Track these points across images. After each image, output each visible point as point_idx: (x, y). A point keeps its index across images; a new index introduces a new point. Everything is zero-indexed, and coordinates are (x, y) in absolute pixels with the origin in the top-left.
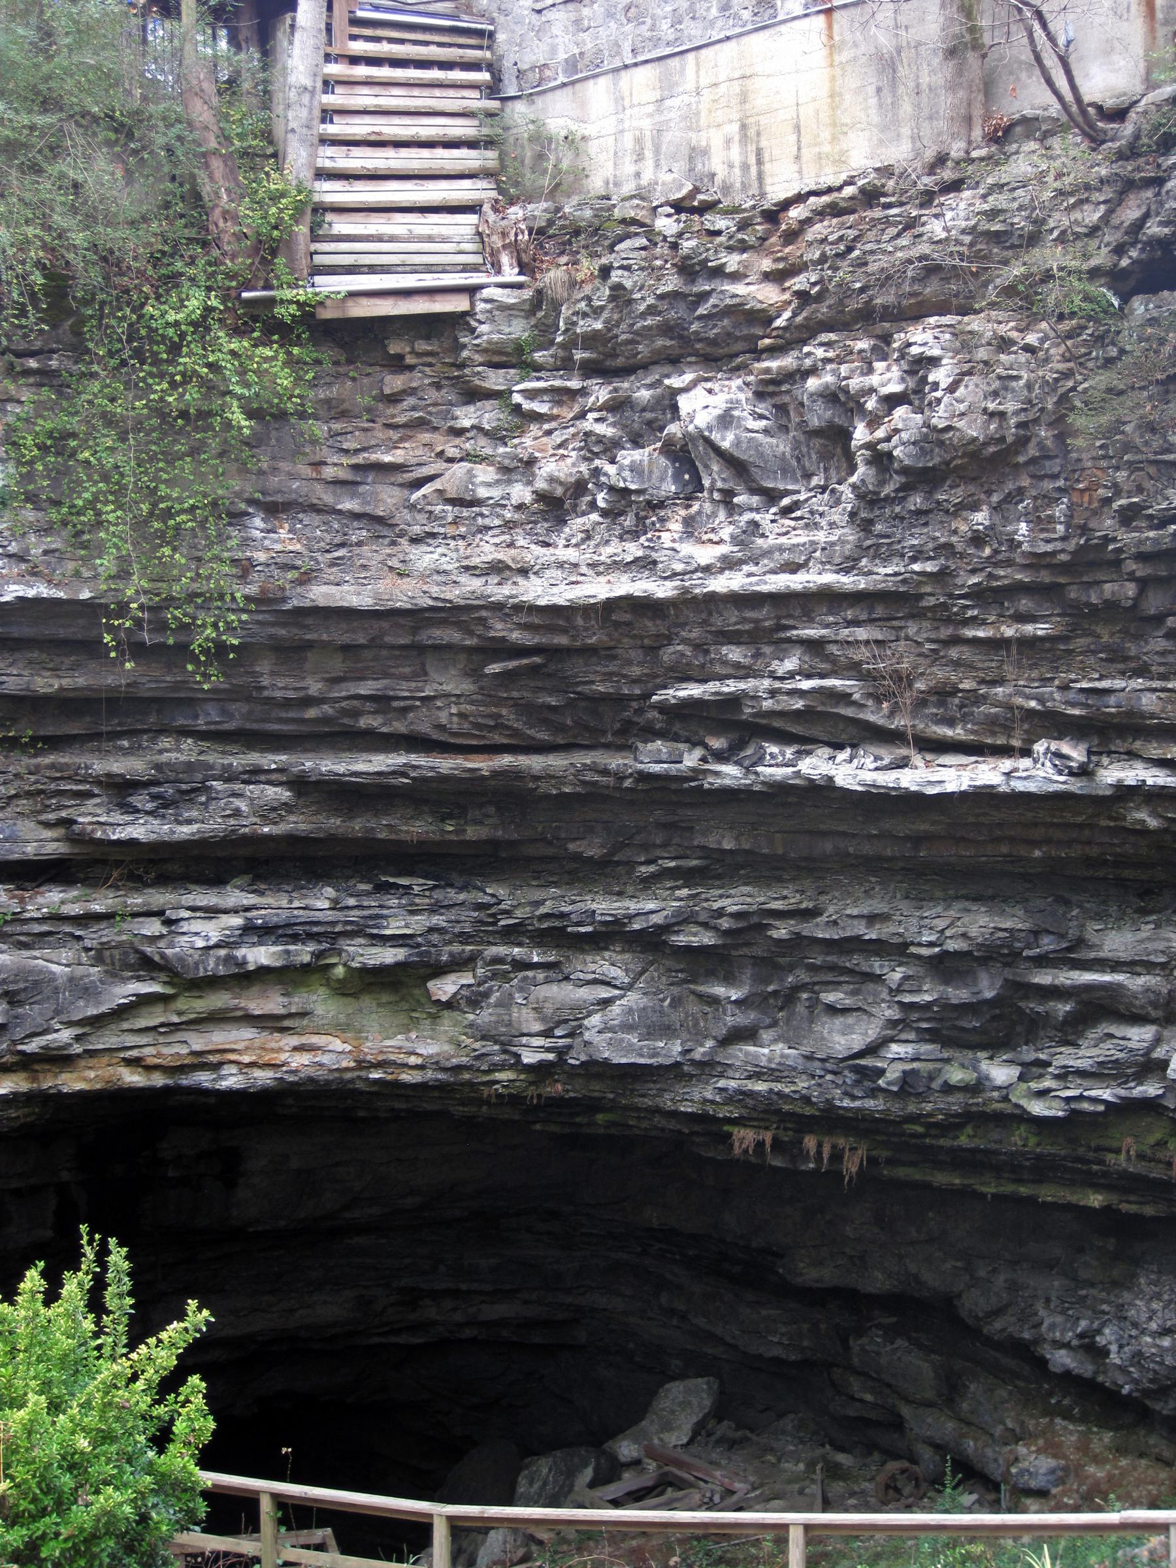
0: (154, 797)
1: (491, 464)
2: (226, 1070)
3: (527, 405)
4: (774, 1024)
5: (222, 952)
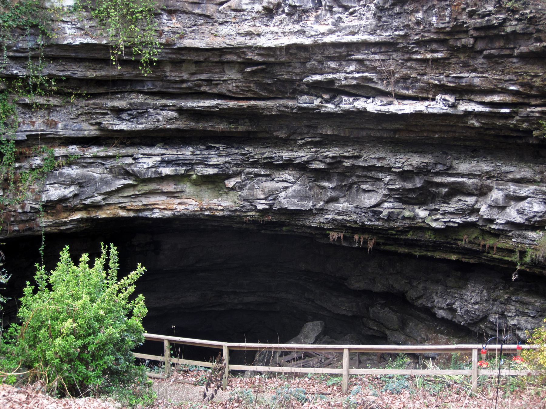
0: (129, 115)
4: (345, 196)
5: (154, 170)
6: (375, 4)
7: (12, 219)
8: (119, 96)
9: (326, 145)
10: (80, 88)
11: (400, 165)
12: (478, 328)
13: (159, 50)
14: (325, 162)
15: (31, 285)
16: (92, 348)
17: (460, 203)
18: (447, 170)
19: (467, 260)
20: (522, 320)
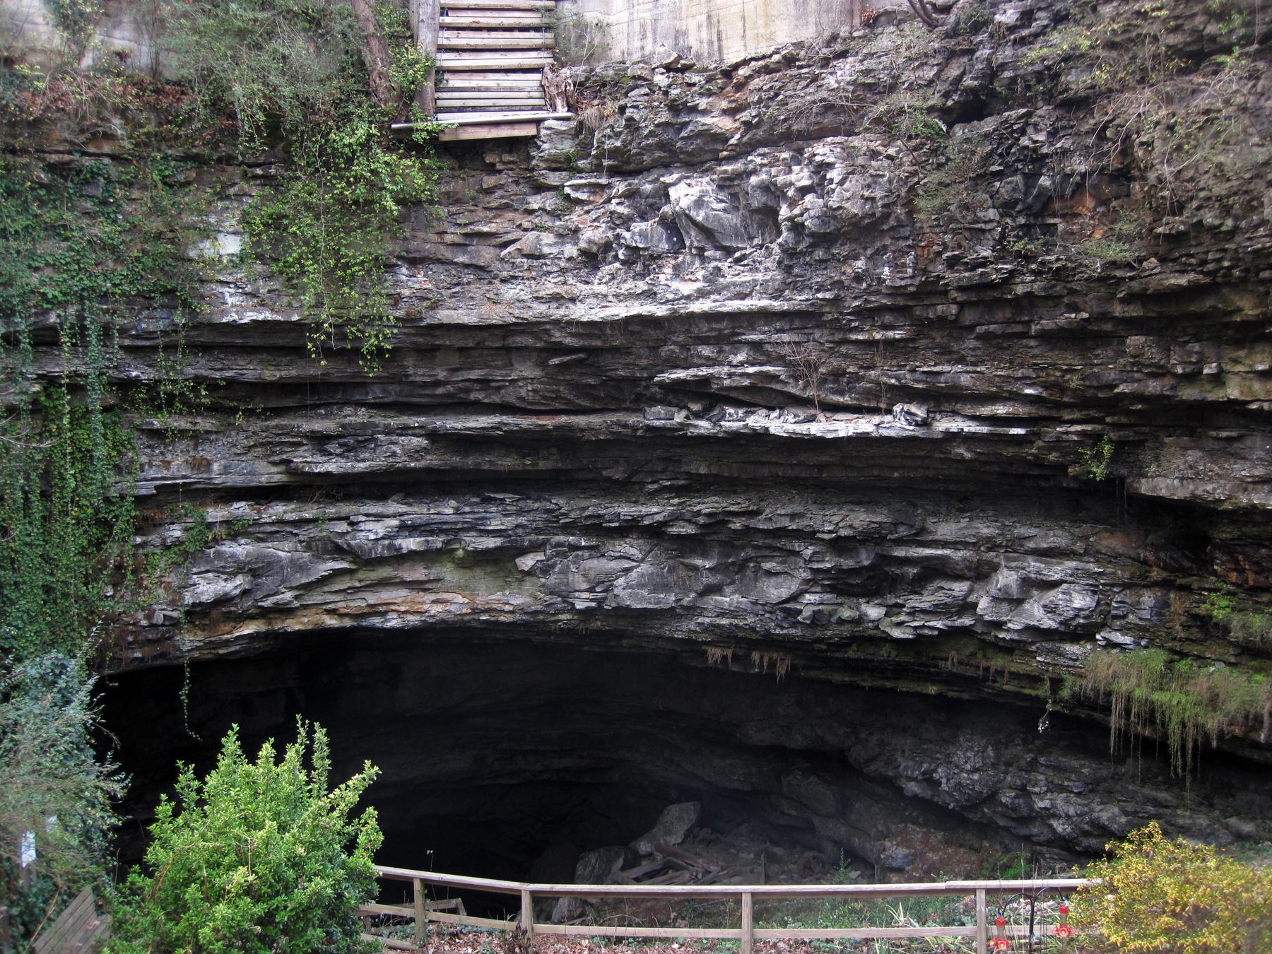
0: (341, 445)
1: (551, 232)
2: (390, 616)
3: (574, 195)
4: (733, 582)
5: (386, 542)
6: (780, 245)
7: (130, 639)
8: (323, 412)
9: (698, 491)
10: (252, 398)
11: (831, 528)
12: (979, 815)
13: (395, 331)
14: (696, 523)
15: (168, 801)
16: (283, 917)
17: (940, 593)
18: (916, 534)
19: (956, 694)
20: (1060, 800)
